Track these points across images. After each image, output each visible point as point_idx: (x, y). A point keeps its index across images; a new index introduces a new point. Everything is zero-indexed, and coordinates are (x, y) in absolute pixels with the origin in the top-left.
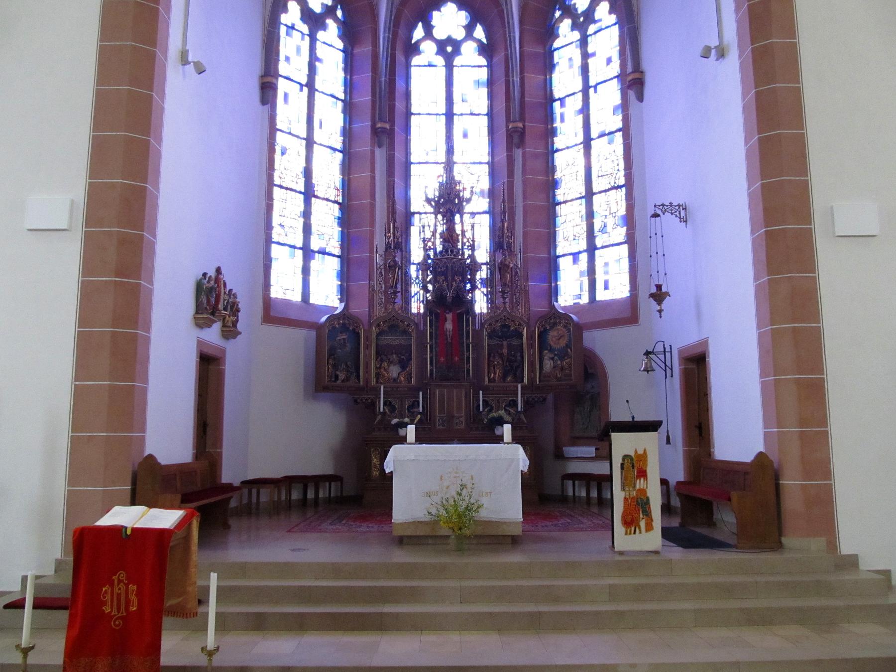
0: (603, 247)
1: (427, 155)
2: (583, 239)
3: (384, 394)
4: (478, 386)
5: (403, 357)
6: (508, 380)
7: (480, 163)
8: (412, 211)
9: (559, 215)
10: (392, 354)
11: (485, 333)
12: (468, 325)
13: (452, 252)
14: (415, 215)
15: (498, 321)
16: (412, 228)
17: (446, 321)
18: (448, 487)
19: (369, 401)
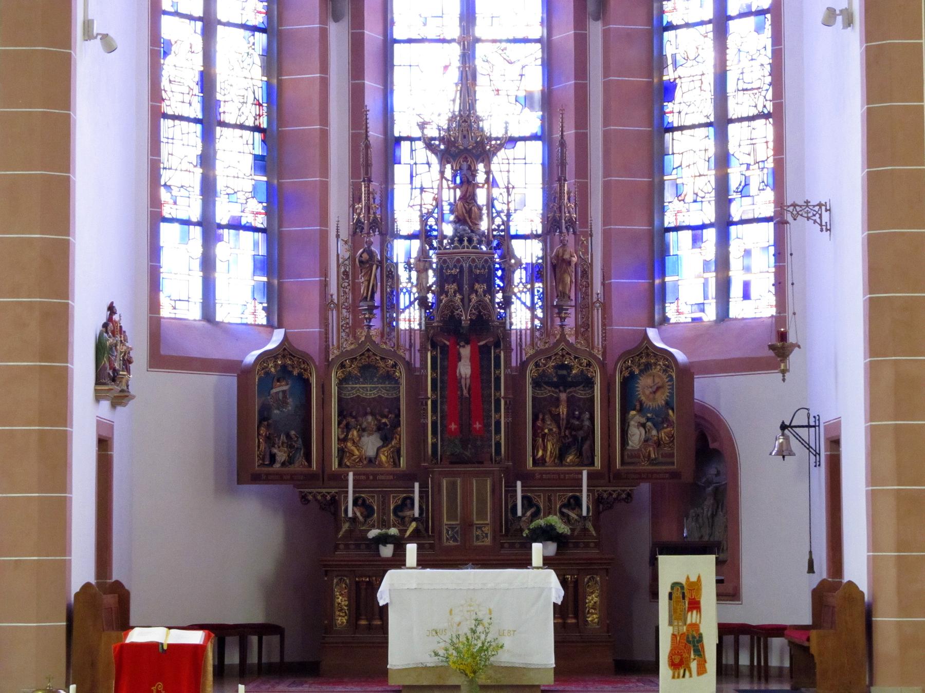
0: (743, 222)
1: (425, 24)
2: (709, 202)
3: (354, 487)
4: (516, 473)
5: (384, 421)
6: (568, 460)
7: (526, 41)
8: (396, 134)
9: (670, 153)
10: (366, 414)
11: (529, 380)
12: (498, 366)
13: (470, 241)
14: (402, 142)
15: (550, 358)
16: (396, 166)
17: (460, 361)
18: (459, 624)
19: (328, 498)
